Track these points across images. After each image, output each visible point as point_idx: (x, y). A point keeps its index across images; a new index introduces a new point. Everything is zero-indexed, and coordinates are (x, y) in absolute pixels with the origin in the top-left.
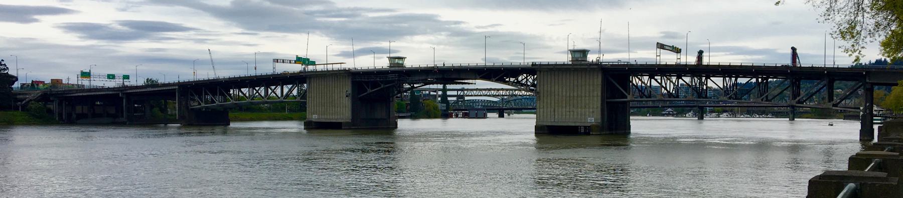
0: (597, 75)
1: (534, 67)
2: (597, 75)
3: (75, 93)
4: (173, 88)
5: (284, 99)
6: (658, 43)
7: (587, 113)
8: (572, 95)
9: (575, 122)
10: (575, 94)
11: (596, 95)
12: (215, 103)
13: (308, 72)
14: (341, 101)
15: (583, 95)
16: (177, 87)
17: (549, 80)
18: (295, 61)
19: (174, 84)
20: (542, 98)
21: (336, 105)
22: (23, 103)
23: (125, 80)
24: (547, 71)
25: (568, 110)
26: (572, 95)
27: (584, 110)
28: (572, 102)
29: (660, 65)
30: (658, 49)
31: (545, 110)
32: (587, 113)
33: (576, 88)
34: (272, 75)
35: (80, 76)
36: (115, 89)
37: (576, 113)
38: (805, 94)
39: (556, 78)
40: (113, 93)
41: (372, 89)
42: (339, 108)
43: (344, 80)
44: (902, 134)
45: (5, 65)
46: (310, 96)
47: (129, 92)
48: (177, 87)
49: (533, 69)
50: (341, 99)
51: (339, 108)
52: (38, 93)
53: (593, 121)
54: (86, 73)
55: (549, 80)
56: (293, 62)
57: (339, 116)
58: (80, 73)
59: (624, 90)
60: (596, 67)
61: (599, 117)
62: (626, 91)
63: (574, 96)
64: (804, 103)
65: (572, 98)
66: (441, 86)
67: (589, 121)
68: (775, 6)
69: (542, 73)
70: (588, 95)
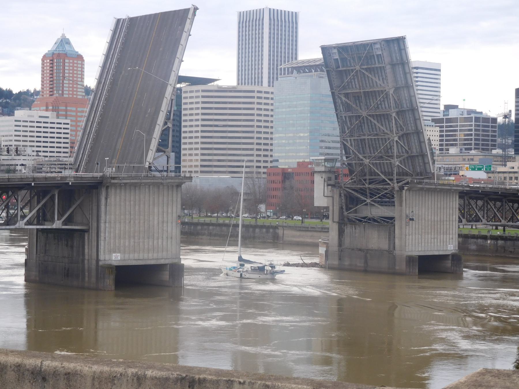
5: (26, 224)
14: (165, 228)
17: (442, 199)
21: (156, 235)
24: (453, 192)
25: (433, 236)
29: (23, 92)
31: (414, 236)
38: (408, 177)
39: (445, 197)
42: (160, 241)
43: (170, 192)
44: (1, 262)
46: (410, 233)
50: (165, 225)
51: (160, 241)
53: (452, 248)
55: (442, 199)
57: (165, 253)
64: (471, 200)
68: (198, 7)
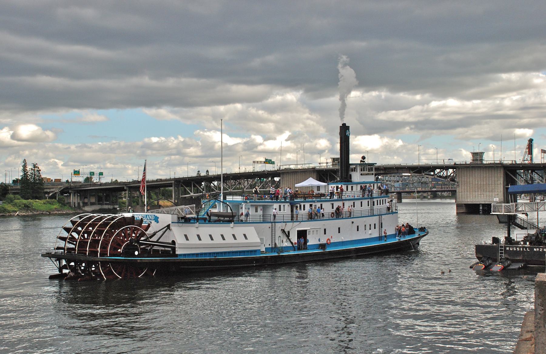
0: (500, 171)
1: (456, 166)
2: (500, 171)
3: (89, 187)
4: (169, 182)
6: (542, 150)
7: (494, 195)
8: (482, 183)
9: (485, 201)
10: (485, 183)
11: (499, 183)
12: (190, 194)
13: (282, 170)
15: (490, 183)
16: (173, 182)
18: (264, 162)
19: (170, 180)
20: (460, 186)
22: (51, 194)
23: (100, 176)
26: (482, 183)
27: (491, 193)
28: (482, 188)
30: (543, 154)
31: (463, 193)
32: (494, 195)
33: (485, 179)
34: (253, 172)
35: (73, 174)
36: (158, 180)
37: (485, 196)
40: (119, 186)
41: (194, 194)
45: (38, 168)
47: (132, 185)
48: (173, 182)
49: (455, 167)
52: (61, 188)
53: (498, 200)
54: (76, 171)
56: (263, 162)
58: (73, 172)
59: (513, 175)
60: (500, 165)
61: (502, 197)
62: (515, 177)
63: (483, 184)
65: (482, 185)
66: (234, 200)
67: (495, 200)
69: (460, 169)
70: (493, 184)
